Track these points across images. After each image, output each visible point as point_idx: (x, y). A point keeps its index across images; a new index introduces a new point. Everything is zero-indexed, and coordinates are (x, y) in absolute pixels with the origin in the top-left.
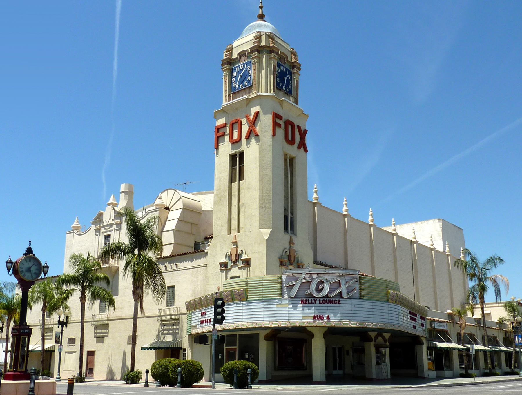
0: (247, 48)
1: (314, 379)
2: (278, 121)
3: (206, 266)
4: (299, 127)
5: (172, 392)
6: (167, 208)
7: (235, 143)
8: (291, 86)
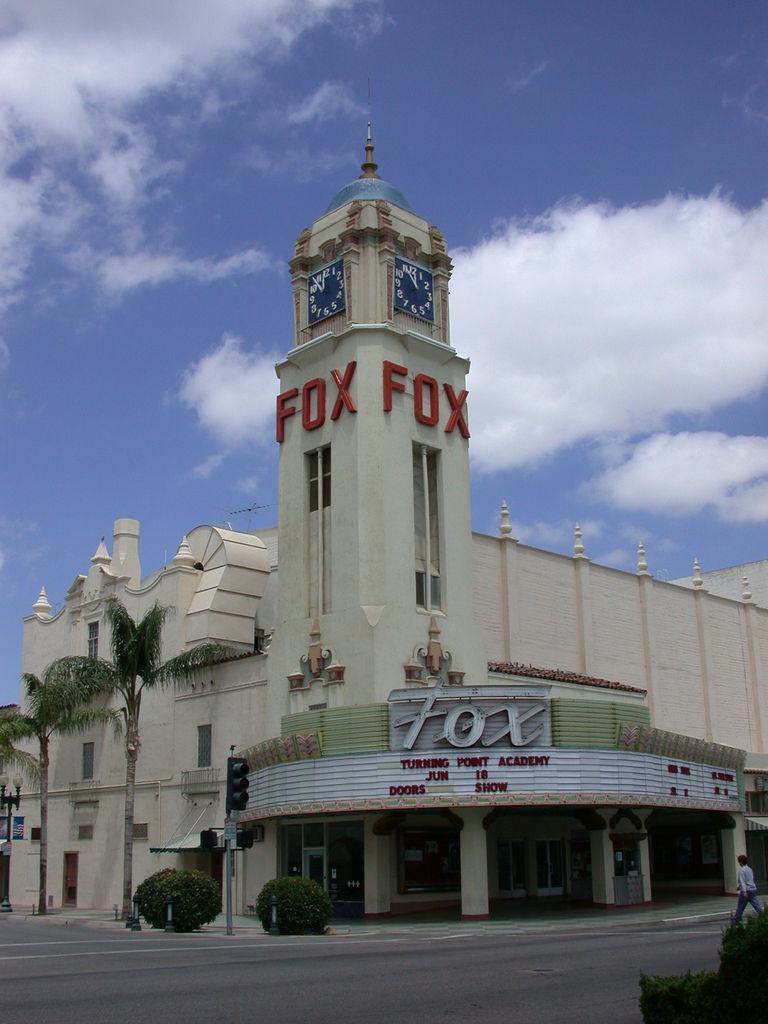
0: (334, 234)
1: (466, 910)
2: (396, 379)
3: (264, 684)
4: (448, 389)
5: (205, 950)
6: (199, 567)
7: (312, 427)
8: (431, 303)
